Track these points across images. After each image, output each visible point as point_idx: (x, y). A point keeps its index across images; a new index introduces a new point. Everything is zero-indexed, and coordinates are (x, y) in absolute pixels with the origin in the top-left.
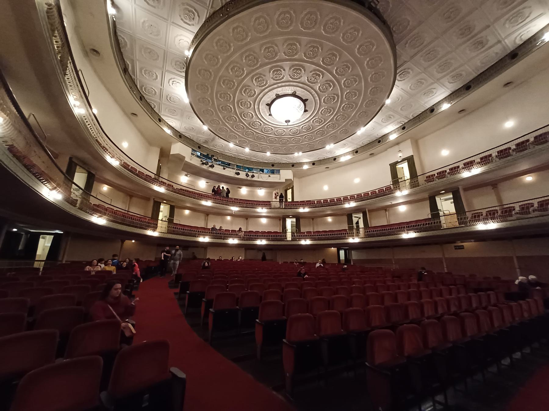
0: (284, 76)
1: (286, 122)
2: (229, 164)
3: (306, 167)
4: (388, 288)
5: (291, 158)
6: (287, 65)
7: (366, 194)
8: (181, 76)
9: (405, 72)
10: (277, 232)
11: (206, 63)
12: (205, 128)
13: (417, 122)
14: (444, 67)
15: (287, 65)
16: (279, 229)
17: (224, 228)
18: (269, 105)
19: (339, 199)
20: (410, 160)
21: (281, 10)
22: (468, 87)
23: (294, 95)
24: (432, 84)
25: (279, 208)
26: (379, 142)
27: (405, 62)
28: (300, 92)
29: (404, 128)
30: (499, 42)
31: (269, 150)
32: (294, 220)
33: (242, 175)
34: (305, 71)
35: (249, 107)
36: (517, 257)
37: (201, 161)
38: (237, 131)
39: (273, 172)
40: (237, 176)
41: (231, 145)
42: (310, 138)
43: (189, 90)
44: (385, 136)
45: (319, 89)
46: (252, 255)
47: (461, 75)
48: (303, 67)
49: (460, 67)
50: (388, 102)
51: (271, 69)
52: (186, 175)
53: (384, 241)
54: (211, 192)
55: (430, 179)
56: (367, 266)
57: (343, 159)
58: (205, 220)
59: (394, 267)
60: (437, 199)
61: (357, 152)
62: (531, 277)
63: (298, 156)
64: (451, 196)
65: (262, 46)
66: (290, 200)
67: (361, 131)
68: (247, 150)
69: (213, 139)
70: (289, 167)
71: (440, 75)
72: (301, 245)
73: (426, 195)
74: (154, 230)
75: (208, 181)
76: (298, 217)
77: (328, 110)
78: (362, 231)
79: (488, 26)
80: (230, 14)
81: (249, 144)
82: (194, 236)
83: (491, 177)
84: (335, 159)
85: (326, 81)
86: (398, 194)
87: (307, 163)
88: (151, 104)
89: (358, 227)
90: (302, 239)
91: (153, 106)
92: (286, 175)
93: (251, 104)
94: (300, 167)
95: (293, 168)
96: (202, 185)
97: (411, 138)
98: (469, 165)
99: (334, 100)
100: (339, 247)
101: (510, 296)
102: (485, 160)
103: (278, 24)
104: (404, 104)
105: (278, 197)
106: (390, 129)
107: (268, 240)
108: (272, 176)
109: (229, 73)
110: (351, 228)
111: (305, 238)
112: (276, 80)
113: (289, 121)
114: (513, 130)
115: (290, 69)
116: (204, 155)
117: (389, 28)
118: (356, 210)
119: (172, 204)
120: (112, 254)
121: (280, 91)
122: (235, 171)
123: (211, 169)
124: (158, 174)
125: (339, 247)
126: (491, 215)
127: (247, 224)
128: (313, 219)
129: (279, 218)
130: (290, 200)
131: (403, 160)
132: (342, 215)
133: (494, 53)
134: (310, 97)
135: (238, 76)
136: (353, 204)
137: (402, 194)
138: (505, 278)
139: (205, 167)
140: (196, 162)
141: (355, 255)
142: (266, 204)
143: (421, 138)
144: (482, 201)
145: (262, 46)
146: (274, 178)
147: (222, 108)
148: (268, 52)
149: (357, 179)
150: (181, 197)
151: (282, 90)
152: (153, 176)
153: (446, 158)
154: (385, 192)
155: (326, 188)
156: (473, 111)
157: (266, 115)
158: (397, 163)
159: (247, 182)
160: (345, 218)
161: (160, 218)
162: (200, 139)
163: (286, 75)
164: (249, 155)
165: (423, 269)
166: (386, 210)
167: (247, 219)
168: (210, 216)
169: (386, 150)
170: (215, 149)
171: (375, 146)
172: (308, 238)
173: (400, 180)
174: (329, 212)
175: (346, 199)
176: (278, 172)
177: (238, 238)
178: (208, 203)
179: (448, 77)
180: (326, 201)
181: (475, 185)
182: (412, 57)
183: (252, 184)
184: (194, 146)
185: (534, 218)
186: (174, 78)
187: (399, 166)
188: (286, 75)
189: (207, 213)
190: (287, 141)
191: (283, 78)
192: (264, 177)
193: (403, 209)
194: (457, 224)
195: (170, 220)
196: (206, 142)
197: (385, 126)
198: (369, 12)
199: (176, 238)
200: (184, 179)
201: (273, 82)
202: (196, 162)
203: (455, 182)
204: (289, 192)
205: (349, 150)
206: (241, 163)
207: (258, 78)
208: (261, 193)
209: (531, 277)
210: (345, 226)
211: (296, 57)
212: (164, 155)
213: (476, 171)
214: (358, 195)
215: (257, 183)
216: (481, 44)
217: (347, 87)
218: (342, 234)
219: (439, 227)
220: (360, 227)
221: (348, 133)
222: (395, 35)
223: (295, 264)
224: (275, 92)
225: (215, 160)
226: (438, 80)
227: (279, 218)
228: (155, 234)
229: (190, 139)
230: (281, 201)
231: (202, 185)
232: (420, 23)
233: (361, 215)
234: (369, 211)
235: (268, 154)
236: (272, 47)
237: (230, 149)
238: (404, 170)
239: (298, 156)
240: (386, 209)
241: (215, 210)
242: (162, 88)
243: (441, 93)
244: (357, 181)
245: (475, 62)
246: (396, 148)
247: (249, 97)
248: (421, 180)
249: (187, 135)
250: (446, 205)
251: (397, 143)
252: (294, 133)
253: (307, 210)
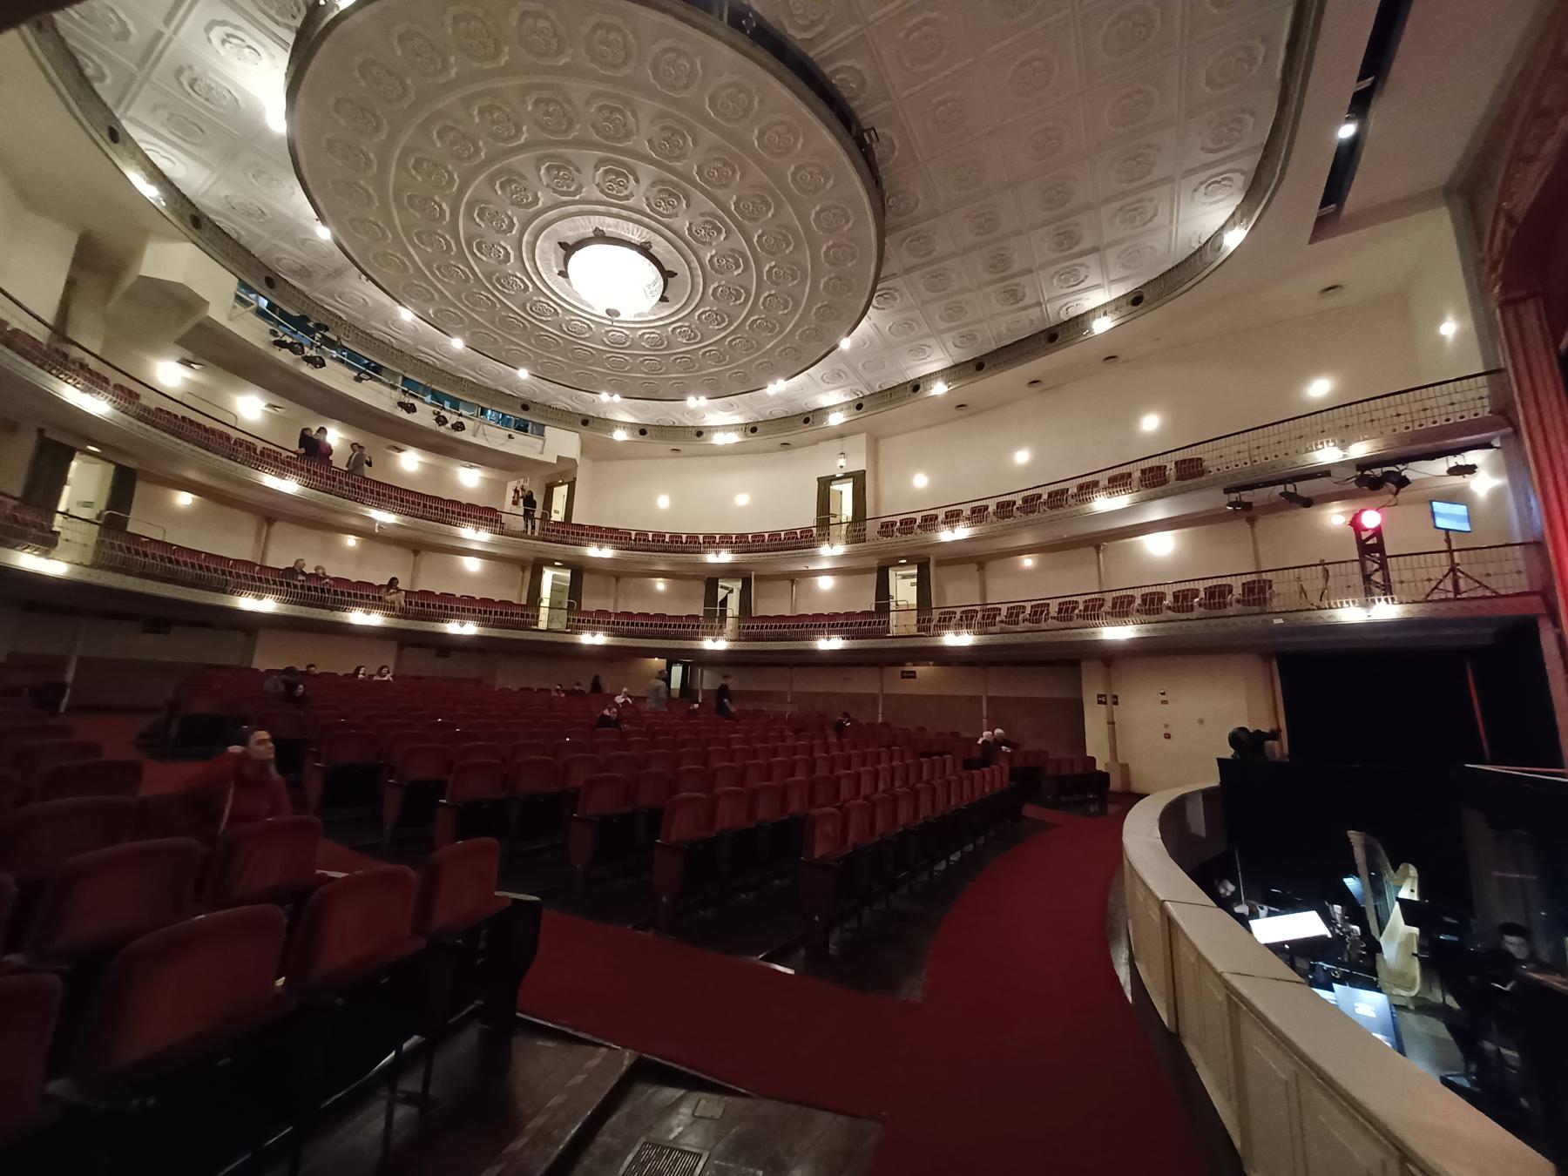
0: (632, 195)
1: (608, 311)
2: (378, 369)
3: (620, 435)
7: (758, 537)
9: (889, 295)
11: (399, 53)
12: (324, 233)
13: (887, 400)
14: (954, 311)
15: (647, 172)
16: (518, 596)
18: (569, 249)
19: (693, 538)
20: (858, 479)
21: (669, 42)
22: (979, 365)
23: (644, 250)
25: (523, 535)
26: (807, 421)
28: (660, 247)
29: (859, 407)
32: (567, 574)
33: (424, 415)
34: (688, 205)
36: (990, 699)
37: (274, 333)
38: (440, 281)
39: (522, 427)
40: (403, 414)
42: (650, 366)
44: (822, 412)
46: (424, 664)
47: (975, 337)
48: (687, 198)
50: (845, 344)
52: (186, 363)
53: (775, 652)
54: (295, 447)
55: (886, 528)
57: (719, 439)
59: (789, 710)
60: (892, 573)
61: (754, 430)
63: (608, 402)
65: (595, 95)
66: (558, 516)
67: (778, 388)
68: (457, 344)
69: (337, 273)
70: (574, 425)
71: (943, 325)
72: (580, 645)
73: (874, 562)
74: (46, 554)
76: (579, 570)
77: (718, 317)
78: (730, 624)
79: (1031, 271)
82: (217, 590)
83: (982, 548)
84: (699, 434)
85: (732, 250)
86: (825, 550)
87: (625, 425)
88: (83, 60)
89: (724, 612)
91: (89, 72)
92: (561, 443)
93: (512, 225)
96: (250, 408)
98: (953, 517)
100: (672, 657)
101: (969, 765)
102: (978, 514)
103: (655, 66)
104: (871, 356)
107: (484, 622)
108: (519, 436)
109: (471, 116)
110: (709, 615)
111: (593, 627)
112: (608, 195)
114: (1028, 469)
115: (653, 184)
116: (284, 315)
118: (730, 572)
119: (132, 464)
121: (610, 226)
123: (306, 370)
124: (60, 328)
126: (966, 620)
128: (618, 579)
129: (518, 563)
130: (558, 516)
131: (846, 476)
132: (696, 578)
133: (1026, 322)
134: (683, 270)
135: (497, 138)
136: (725, 557)
137: (832, 551)
138: (964, 734)
139: (284, 356)
140: (253, 331)
142: (485, 515)
143: (884, 437)
144: (957, 592)
145: (595, 95)
146: (522, 445)
147: (410, 198)
149: (749, 497)
150: (157, 445)
151: (616, 226)
152: (41, 334)
154: (801, 541)
155: (663, 502)
156: (980, 412)
157: (549, 269)
158: (833, 479)
160: (700, 588)
161: (61, 508)
162: (285, 257)
163: (639, 193)
164: (457, 357)
165: (846, 715)
166: (793, 582)
167: (416, 552)
168: (277, 526)
169: (816, 443)
170: (330, 303)
171: (796, 427)
174: (662, 568)
175: (711, 542)
177: (385, 608)
178: (289, 486)
179: (954, 333)
180: (659, 536)
181: (957, 557)
182: (908, 271)
183: (443, 447)
184: (247, 272)
185: (1021, 634)
186: (237, 28)
187: (835, 487)
188: (639, 193)
189: (271, 512)
190: (585, 354)
191: (626, 198)
192: (495, 438)
193: (826, 583)
194: (914, 630)
195: (113, 521)
196: (305, 273)
197: (828, 390)
198: (855, 150)
199: (139, 589)
200: (170, 374)
201: (597, 194)
202: (253, 331)
204: (560, 493)
208: (469, 479)
211: (678, 165)
212: (97, 263)
213: (962, 532)
216: (1013, 295)
218: (690, 627)
219: (883, 633)
220: (729, 613)
221: (749, 384)
222: (889, 215)
223: (554, 694)
227: (518, 563)
228: (55, 567)
230: (528, 515)
231: (250, 408)
232: (936, 214)
233: (737, 585)
234: (759, 578)
235: (523, 374)
237: (402, 327)
238: (844, 493)
239: (608, 402)
240: (793, 578)
242: (168, 32)
243: (936, 362)
244: (742, 500)
246: (837, 443)
247: (513, 203)
248: (872, 528)
249: (225, 225)
250: (904, 589)
251: (841, 434)
252: (617, 343)
253: (607, 553)
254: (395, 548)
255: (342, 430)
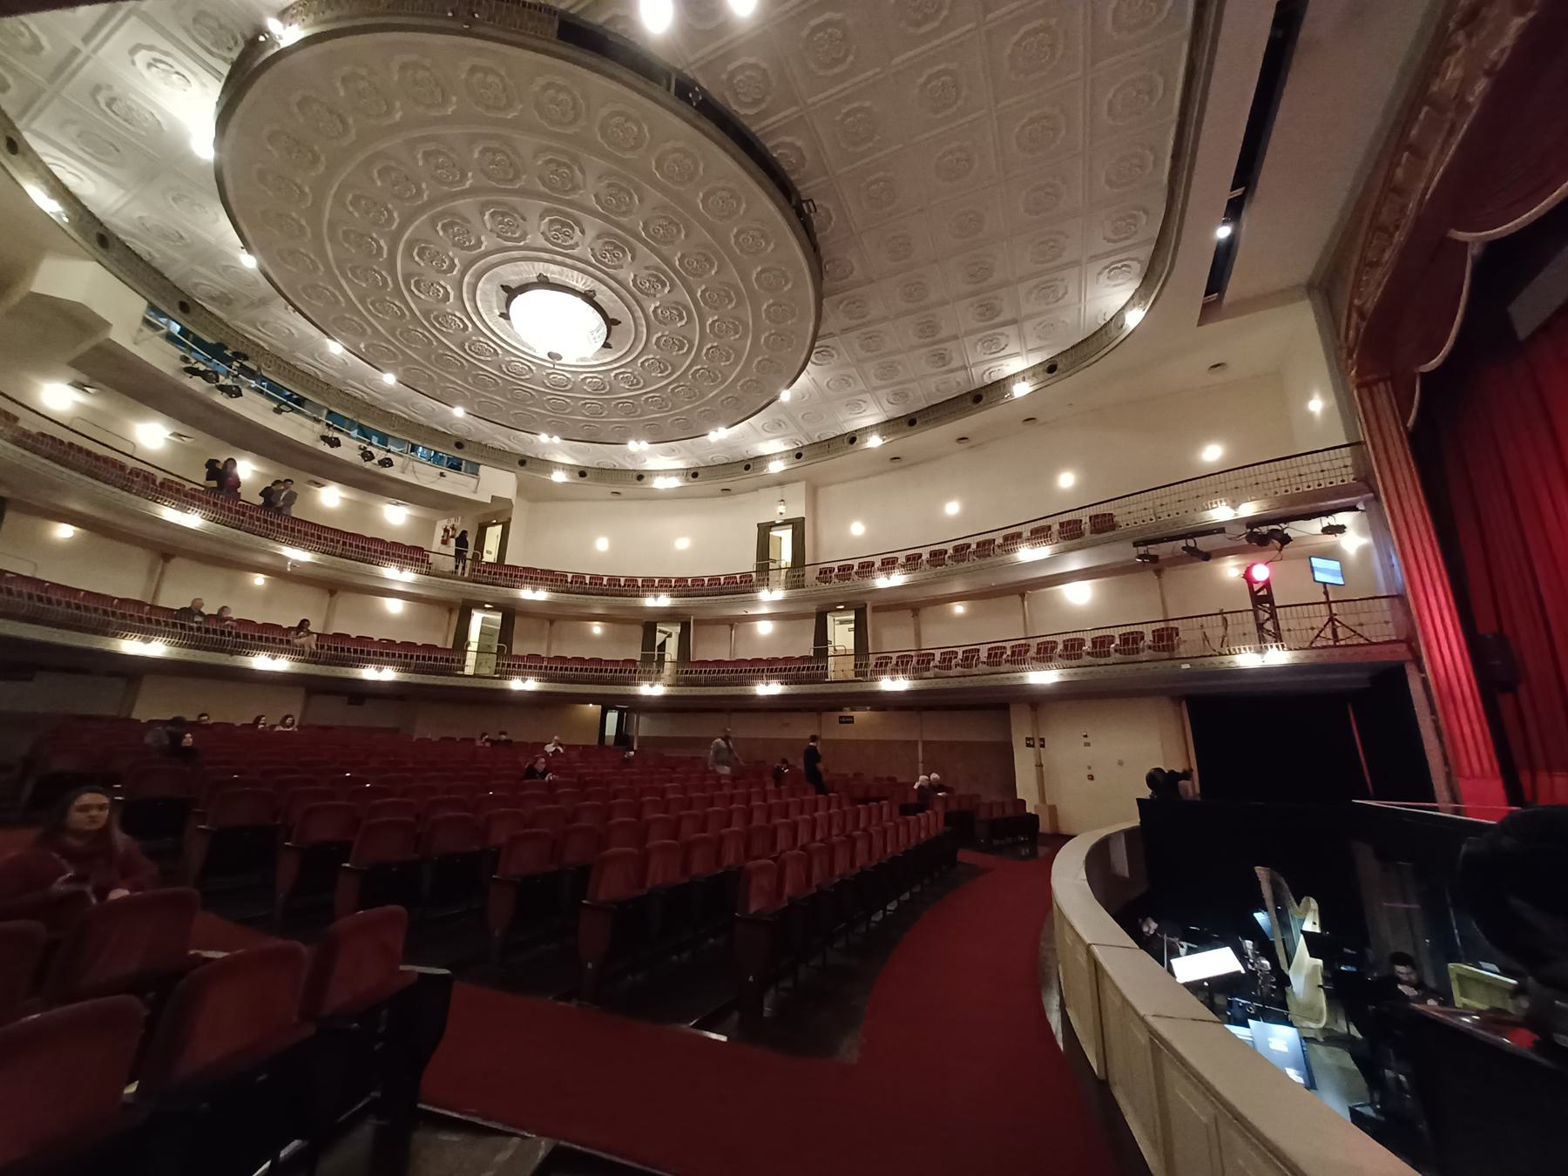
0: (577, 244)
2: (300, 401)
3: (559, 477)
4: (690, 804)
5: (521, 441)
6: (593, 225)
8: (216, 73)
9: (827, 352)
10: (435, 647)
11: (342, 93)
12: (249, 262)
13: (824, 451)
14: (888, 371)
15: (593, 225)
16: (442, 638)
17: (235, 614)
18: (511, 292)
19: (631, 581)
20: (797, 526)
22: (911, 421)
23: (589, 297)
24: (863, 392)
25: (452, 575)
26: (747, 467)
27: (831, 335)
28: (604, 296)
30: (965, 368)
31: (465, 402)
32: (497, 617)
33: (349, 450)
34: (633, 258)
35: (445, 272)
36: (925, 743)
39: (455, 466)
40: (326, 448)
41: (335, 348)
42: (591, 410)
43: (232, 130)
45: (655, 311)
46: (332, 713)
48: (633, 250)
49: (909, 381)
50: (785, 396)
51: (547, 212)
53: (712, 697)
55: (825, 575)
56: (668, 753)
57: (660, 483)
58: (151, 572)
60: (830, 618)
61: (695, 475)
62: (934, 776)
63: (548, 443)
64: (852, 617)
66: (490, 555)
67: (719, 435)
68: (389, 379)
69: (263, 302)
71: (877, 383)
72: (509, 691)
73: (813, 608)
75: (184, 429)
76: (511, 613)
77: (662, 365)
80: (477, 29)
81: (402, 364)
82: (96, 632)
84: (640, 477)
86: (764, 595)
87: (564, 467)
90: (511, 673)
92: (496, 483)
94: (537, 471)
95: (523, 471)
96: (151, 436)
97: (807, 480)
98: (888, 565)
99: (681, 348)
101: (905, 810)
102: (912, 562)
104: (809, 409)
105: (453, 541)
106: (773, 447)
107: (405, 667)
110: (647, 659)
111: (524, 674)
113: (560, 358)
115: (598, 237)
117: (819, 260)
118: (669, 616)
120: (1148, 770)
121: (554, 272)
122: (320, 429)
123: (220, 399)
125: (607, 703)
126: (901, 665)
127: (331, 609)
128: (552, 622)
129: (447, 605)
130: (490, 555)
131: (786, 523)
136: (664, 601)
137: (771, 596)
139: (196, 384)
141: (643, 727)
142: (410, 554)
144: (893, 637)
146: (455, 484)
148: (555, 172)
149: (686, 542)
151: (561, 274)
153: (857, 540)
154: (740, 586)
157: (491, 311)
158: (773, 525)
159: (361, 476)
160: (638, 632)
162: (202, 282)
163: (584, 243)
164: (388, 392)
166: (732, 626)
167: (332, 593)
170: (251, 332)
172: (531, 674)
173: (772, 566)
175: (650, 585)
176: (474, 471)
180: (596, 579)
181: (893, 604)
182: (845, 331)
186: (167, 54)
187: (774, 533)
188: (584, 243)
191: (572, 247)
192: (425, 475)
193: (765, 628)
194: (851, 676)
197: (768, 439)
201: (542, 242)
202: (161, 357)
203: (860, 593)
204: (493, 534)
205: (680, 464)
206: (346, 409)
207: (504, 215)
208: (395, 517)
209: (934, 776)
210: (636, 653)
211: (623, 220)
213: (897, 579)
214: (679, 580)
215: (394, 486)
216: (941, 358)
217: (716, 335)
218: (628, 672)
219: (821, 678)
220: (667, 658)
224: (540, 268)
225: (244, 370)
226: (875, 389)
227: (447, 605)
229: (148, 265)
230: (459, 555)
234: (698, 622)
235: (459, 412)
236: (569, 167)
239: (548, 443)
240: (732, 622)
241: (216, 548)
243: (870, 416)
244: (683, 544)
245: (932, 386)
246: (777, 490)
247: (454, 245)
248: (811, 574)
250: (841, 635)
251: (781, 482)
253: (542, 595)
254: (303, 587)
255: (257, 462)
